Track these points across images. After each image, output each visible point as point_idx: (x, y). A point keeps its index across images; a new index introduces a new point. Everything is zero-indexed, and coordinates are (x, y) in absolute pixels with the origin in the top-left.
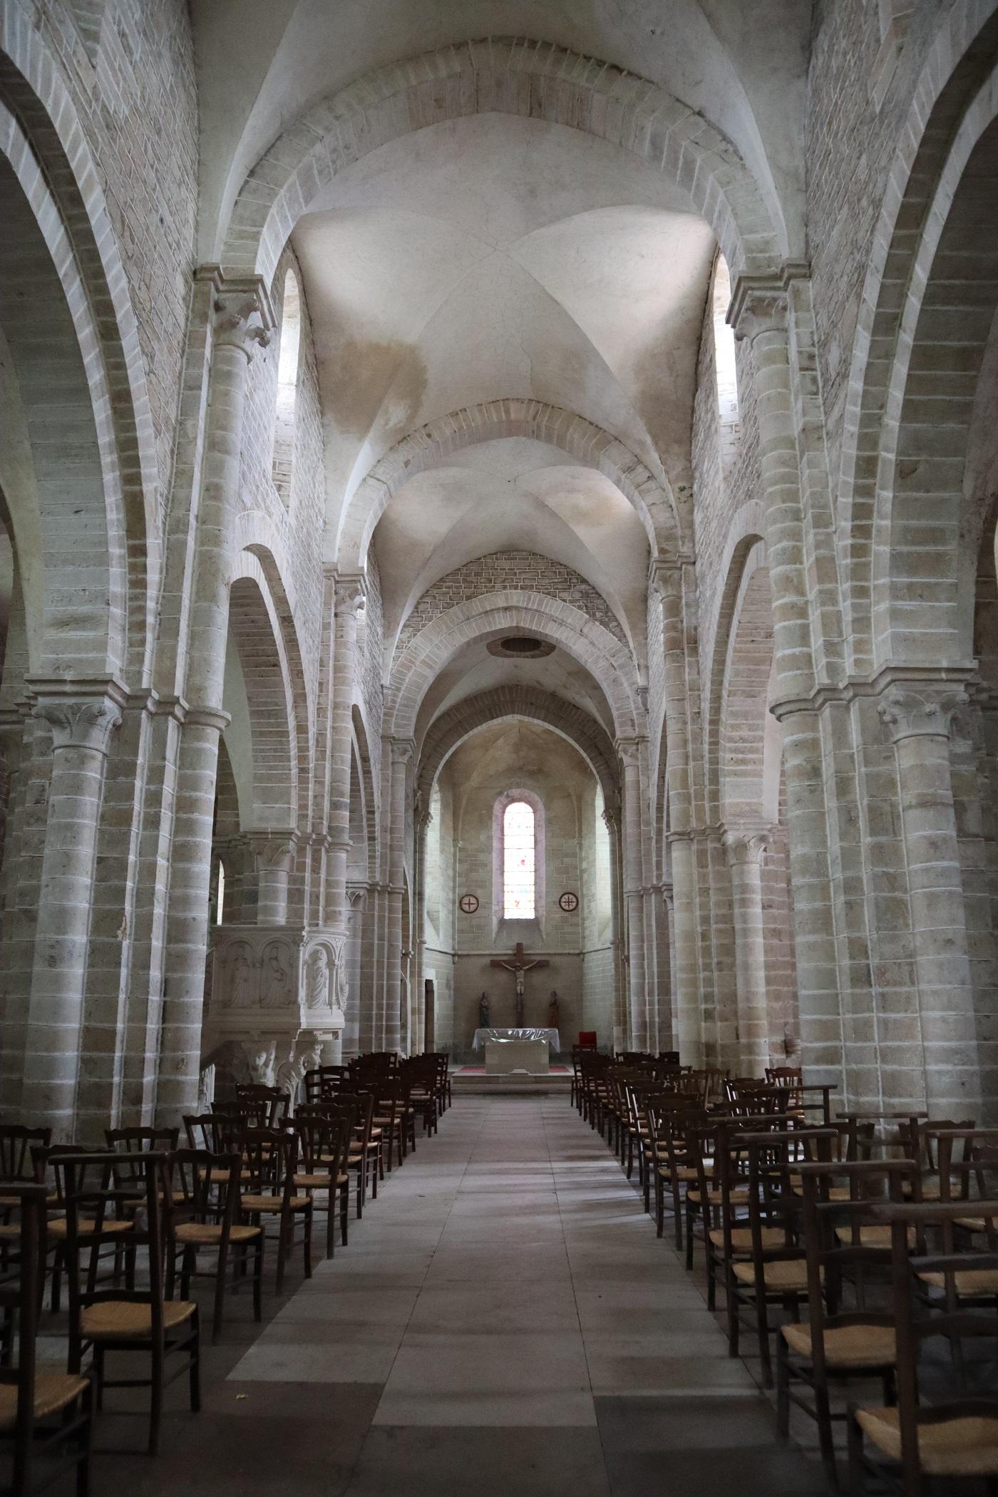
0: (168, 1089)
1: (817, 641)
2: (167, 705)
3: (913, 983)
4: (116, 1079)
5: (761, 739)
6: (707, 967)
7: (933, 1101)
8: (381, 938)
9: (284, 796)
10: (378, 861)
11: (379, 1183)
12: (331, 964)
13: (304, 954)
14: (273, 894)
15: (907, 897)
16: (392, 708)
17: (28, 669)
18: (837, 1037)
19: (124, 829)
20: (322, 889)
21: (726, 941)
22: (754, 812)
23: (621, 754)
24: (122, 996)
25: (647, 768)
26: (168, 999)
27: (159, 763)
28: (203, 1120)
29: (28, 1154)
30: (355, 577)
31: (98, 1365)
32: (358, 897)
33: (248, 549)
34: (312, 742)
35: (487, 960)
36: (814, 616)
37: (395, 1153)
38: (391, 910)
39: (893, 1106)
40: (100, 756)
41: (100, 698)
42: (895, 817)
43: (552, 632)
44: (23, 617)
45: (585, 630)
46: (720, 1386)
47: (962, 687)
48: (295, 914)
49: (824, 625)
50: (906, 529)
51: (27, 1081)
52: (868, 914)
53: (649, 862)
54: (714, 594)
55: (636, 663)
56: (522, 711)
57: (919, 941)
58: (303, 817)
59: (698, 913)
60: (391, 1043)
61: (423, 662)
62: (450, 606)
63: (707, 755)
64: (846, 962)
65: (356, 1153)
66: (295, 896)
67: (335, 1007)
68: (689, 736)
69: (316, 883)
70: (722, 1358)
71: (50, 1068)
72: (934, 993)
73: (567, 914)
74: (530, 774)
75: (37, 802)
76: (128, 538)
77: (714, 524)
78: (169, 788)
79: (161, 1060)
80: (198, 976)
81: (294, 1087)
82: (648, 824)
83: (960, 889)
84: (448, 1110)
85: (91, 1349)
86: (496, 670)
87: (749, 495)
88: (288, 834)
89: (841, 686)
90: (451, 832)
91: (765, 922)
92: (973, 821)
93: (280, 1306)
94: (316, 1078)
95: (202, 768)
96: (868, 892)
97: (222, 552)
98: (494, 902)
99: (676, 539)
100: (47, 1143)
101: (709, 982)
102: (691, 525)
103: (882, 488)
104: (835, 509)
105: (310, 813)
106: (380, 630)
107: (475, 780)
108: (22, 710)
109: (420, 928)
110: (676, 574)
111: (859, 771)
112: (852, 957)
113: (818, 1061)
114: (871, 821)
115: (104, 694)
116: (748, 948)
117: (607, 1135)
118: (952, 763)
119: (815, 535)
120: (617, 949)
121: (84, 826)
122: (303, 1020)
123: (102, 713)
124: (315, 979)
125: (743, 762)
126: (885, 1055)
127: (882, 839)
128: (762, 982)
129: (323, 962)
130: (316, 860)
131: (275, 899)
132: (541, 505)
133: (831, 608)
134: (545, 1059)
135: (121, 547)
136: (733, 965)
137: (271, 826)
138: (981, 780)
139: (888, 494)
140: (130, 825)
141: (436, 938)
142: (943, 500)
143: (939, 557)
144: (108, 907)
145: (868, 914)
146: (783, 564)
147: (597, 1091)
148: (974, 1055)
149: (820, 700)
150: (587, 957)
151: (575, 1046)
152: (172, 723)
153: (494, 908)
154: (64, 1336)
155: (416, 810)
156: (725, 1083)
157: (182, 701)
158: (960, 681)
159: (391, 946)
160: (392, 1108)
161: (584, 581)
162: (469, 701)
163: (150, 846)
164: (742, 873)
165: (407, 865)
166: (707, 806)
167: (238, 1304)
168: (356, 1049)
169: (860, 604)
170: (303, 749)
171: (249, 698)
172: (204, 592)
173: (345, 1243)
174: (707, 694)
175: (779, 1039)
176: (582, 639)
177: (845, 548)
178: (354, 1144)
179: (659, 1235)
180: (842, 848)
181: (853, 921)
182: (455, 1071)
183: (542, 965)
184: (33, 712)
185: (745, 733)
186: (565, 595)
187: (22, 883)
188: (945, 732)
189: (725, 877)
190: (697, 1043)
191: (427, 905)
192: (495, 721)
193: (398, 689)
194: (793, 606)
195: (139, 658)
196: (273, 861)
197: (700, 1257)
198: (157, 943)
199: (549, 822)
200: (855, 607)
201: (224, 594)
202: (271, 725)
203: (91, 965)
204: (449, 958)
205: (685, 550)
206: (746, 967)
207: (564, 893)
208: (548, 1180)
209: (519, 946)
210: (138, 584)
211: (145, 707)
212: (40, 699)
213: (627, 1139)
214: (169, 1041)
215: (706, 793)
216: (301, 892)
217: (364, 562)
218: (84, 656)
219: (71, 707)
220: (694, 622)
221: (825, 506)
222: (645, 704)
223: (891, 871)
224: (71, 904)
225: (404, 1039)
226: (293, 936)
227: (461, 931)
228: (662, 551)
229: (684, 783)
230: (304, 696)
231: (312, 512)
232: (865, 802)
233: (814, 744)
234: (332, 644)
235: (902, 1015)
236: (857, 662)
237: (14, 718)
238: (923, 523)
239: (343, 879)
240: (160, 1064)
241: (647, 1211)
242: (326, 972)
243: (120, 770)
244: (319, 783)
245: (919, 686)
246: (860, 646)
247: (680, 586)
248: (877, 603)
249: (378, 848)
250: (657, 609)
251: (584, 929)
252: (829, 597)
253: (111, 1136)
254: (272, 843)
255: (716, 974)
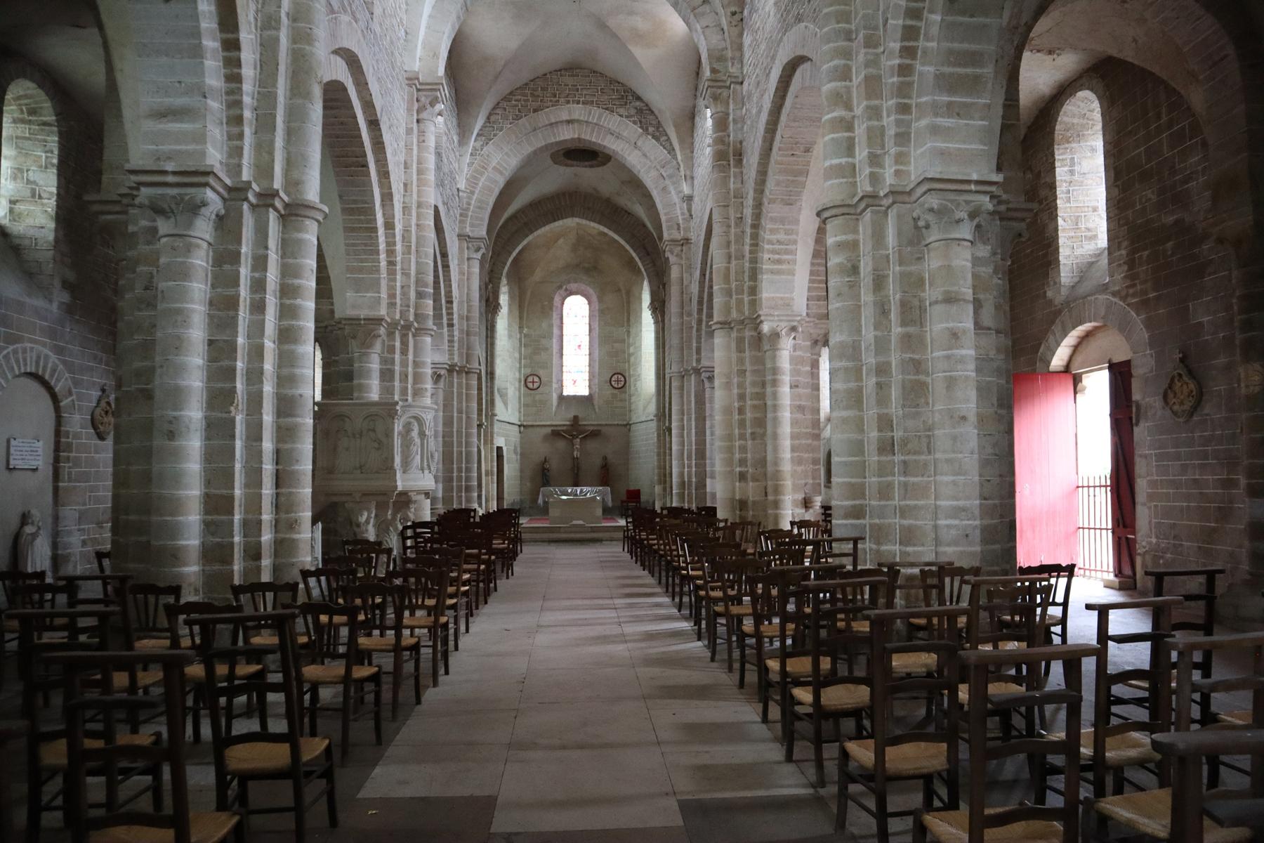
0: (283, 546)
1: (861, 153)
2: (267, 197)
3: (930, 452)
4: (237, 539)
5: (795, 242)
6: (742, 437)
7: (941, 549)
8: (460, 412)
9: (375, 285)
10: (456, 345)
11: (471, 619)
12: (422, 434)
13: (398, 427)
14: (366, 374)
15: (929, 380)
16: (468, 209)
17: (128, 161)
18: (863, 496)
19: (231, 313)
20: (410, 369)
21: (758, 415)
22: (788, 304)
23: (668, 254)
24: (238, 466)
25: (690, 267)
26: (280, 467)
27: (261, 252)
28: (317, 573)
29: (161, 608)
30: (432, 87)
31: (242, 798)
32: (439, 376)
33: (336, 52)
34: (398, 238)
35: (549, 430)
36: (860, 131)
37: (481, 592)
38: (468, 387)
39: (908, 554)
40: (205, 245)
41: (202, 189)
42: (922, 310)
43: (611, 144)
44: (119, 110)
45: (639, 143)
46: (782, 786)
47: (988, 199)
48: (387, 390)
49: (869, 138)
50: (951, 52)
51: (154, 543)
52: (895, 393)
53: (690, 348)
54: (759, 112)
55: (682, 173)
56: (574, 215)
57: (937, 417)
58: (392, 305)
59: (735, 391)
60: (469, 500)
61: (495, 168)
62: (518, 118)
63: (747, 255)
64: (874, 434)
65: (451, 596)
66: (387, 375)
67: (426, 472)
68: (732, 238)
69: (404, 364)
70: (779, 763)
71: (174, 531)
72: (947, 461)
73: (616, 391)
74: (587, 271)
75: (146, 288)
76: (221, 31)
77: (763, 47)
78: (272, 276)
79: (277, 521)
80: (306, 447)
81: (393, 542)
82: (690, 315)
83: (974, 374)
84: (520, 556)
85: (235, 783)
86: (556, 178)
87: (799, 19)
88: (379, 321)
89: (882, 194)
90: (517, 320)
91: (792, 400)
92: (988, 318)
93: (398, 730)
94: (409, 533)
95: (303, 257)
96: (897, 377)
97: (314, 50)
98: (554, 380)
99: (726, 60)
100: (178, 599)
101: (743, 449)
102: (740, 47)
103: (931, 11)
104: (885, 31)
105: (398, 301)
106: (456, 138)
107: (538, 275)
108: (125, 201)
109: (492, 403)
110: (725, 94)
111: (894, 270)
112: (880, 430)
113: (846, 516)
114: (903, 313)
115: (206, 185)
116: (776, 421)
117: (657, 575)
118: (974, 265)
119: (866, 54)
120: (659, 420)
121: (193, 310)
122: (399, 483)
123: (204, 204)
124: (408, 447)
125: (779, 262)
126: (904, 512)
127: (911, 329)
128: (788, 449)
129: (415, 434)
130: (405, 344)
131: (369, 377)
132: (602, 26)
133: (876, 123)
134: (599, 512)
135: (214, 40)
136: (764, 434)
137: (363, 313)
138: (996, 281)
139: (937, 18)
140: (237, 310)
141: (507, 411)
142: (985, 26)
143: (977, 79)
144: (220, 385)
145: (895, 393)
146: (835, 80)
147: (648, 539)
148: (977, 512)
149: (862, 205)
150: (633, 428)
151: (623, 502)
152: (272, 215)
153: (555, 386)
154: (208, 764)
155: (487, 301)
156: (760, 534)
157: (282, 194)
158: (985, 193)
159: (468, 418)
160: (477, 557)
161: (639, 98)
162: (534, 205)
163: (257, 329)
164: (774, 358)
165: (479, 351)
166: (746, 299)
167: (362, 729)
168: (440, 506)
169: (902, 121)
170: (391, 244)
171: (340, 197)
172: (298, 89)
173: (447, 673)
174: (749, 201)
175: (800, 496)
176: (636, 151)
177: (892, 67)
178: (451, 590)
179: (713, 660)
180: (876, 337)
181: (882, 400)
182: (524, 521)
183: (595, 434)
184: (137, 201)
185: (781, 236)
186: (622, 111)
187: (137, 364)
188: (969, 237)
189: (759, 361)
190: (732, 500)
191: (498, 383)
192: (557, 224)
193: (472, 193)
194: (842, 119)
195: (238, 152)
196: (367, 344)
197: (752, 677)
198: (268, 418)
199: (602, 312)
200: (898, 123)
201: (317, 92)
202: (360, 221)
203: (208, 438)
204: (516, 428)
205: (733, 70)
206: (775, 436)
207: (613, 372)
208: (613, 614)
209: (576, 418)
210: (234, 78)
211: (246, 199)
212: (143, 189)
213: (677, 581)
214: (282, 505)
215: (746, 288)
216: (392, 372)
217: (441, 71)
218: (183, 147)
219: (174, 197)
220: (740, 137)
221: (876, 28)
222: (689, 210)
223: (916, 357)
224: (185, 383)
225: (480, 497)
226: (387, 410)
227: (526, 405)
228: (713, 71)
229: (727, 278)
230: (391, 195)
231: (394, 22)
232: (898, 296)
233: (854, 245)
234: (415, 148)
235: (920, 479)
236: (898, 173)
237: (117, 208)
238: (965, 46)
239: (429, 360)
240: (277, 525)
241: (699, 639)
242: (418, 441)
243: (225, 258)
244: (406, 274)
245: (952, 196)
246: (900, 158)
247: (728, 104)
248: (918, 119)
249: (456, 333)
250: (707, 120)
251: (630, 404)
252: (874, 113)
253: (237, 590)
254: (365, 328)
255: (750, 442)
